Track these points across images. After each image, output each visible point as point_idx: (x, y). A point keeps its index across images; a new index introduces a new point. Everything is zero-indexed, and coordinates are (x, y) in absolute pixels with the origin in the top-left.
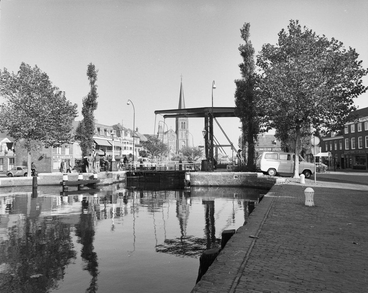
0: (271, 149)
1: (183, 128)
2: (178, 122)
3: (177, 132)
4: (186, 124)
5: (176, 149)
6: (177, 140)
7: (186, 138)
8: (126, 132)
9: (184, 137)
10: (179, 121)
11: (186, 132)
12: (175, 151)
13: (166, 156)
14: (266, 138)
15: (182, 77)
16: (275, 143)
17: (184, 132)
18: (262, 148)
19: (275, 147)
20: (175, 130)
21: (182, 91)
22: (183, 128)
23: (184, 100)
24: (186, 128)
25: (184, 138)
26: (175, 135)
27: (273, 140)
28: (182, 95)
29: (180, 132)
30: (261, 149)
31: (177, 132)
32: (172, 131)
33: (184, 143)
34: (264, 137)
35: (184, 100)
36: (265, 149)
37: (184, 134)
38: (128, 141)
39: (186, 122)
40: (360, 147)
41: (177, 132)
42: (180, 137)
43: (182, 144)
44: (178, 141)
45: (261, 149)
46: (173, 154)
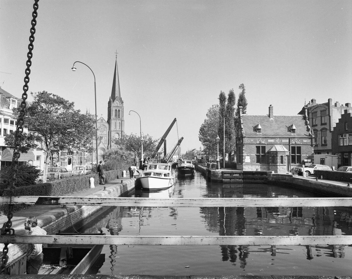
0: (287, 141)
1: (117, 116)
2: (110, 110)
3: (109, 121)
4: (121, 112)
5: (107, 143)
6: (109, 132)
7: (120, 130)
8: (8, 99)
9: (118, 127)
10: (112, 108)
11: (120, 121)
12: (106, 145)
13: (90, 150)
14: (276, 121)
15: (117, 54)
16: (293, 131)
17: (118, 122)
18: (272, 138)
19: (294, 138)
20: (106, 120)
21: (117, 71)
22: (117, 116)
23: (118, 75)
24: (121, 116)
25: (118, 130)
26: (107, 125)
27: (288, 125)
28: (116, 66)
29: (113, 122)
30: (270, 141)
31: (109, 122)
32: (102, 120)
33: (117, 135)
34: (271, 119)
35: (118, 75)
36: (278, 141)
37: (118, 125)
38: (6, 117)
39: (121, 110)
40: (292, 147)
41: (109, 122)
42: (113, 128)
43: (115, 136)
44: (111, 133)
45: (270, 141)
46: (103, 149)
